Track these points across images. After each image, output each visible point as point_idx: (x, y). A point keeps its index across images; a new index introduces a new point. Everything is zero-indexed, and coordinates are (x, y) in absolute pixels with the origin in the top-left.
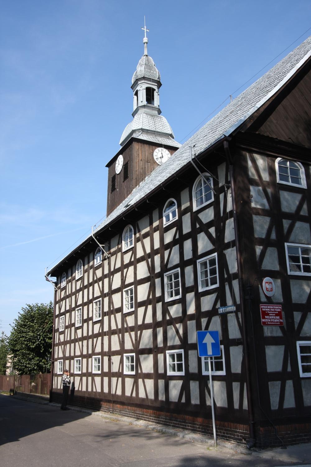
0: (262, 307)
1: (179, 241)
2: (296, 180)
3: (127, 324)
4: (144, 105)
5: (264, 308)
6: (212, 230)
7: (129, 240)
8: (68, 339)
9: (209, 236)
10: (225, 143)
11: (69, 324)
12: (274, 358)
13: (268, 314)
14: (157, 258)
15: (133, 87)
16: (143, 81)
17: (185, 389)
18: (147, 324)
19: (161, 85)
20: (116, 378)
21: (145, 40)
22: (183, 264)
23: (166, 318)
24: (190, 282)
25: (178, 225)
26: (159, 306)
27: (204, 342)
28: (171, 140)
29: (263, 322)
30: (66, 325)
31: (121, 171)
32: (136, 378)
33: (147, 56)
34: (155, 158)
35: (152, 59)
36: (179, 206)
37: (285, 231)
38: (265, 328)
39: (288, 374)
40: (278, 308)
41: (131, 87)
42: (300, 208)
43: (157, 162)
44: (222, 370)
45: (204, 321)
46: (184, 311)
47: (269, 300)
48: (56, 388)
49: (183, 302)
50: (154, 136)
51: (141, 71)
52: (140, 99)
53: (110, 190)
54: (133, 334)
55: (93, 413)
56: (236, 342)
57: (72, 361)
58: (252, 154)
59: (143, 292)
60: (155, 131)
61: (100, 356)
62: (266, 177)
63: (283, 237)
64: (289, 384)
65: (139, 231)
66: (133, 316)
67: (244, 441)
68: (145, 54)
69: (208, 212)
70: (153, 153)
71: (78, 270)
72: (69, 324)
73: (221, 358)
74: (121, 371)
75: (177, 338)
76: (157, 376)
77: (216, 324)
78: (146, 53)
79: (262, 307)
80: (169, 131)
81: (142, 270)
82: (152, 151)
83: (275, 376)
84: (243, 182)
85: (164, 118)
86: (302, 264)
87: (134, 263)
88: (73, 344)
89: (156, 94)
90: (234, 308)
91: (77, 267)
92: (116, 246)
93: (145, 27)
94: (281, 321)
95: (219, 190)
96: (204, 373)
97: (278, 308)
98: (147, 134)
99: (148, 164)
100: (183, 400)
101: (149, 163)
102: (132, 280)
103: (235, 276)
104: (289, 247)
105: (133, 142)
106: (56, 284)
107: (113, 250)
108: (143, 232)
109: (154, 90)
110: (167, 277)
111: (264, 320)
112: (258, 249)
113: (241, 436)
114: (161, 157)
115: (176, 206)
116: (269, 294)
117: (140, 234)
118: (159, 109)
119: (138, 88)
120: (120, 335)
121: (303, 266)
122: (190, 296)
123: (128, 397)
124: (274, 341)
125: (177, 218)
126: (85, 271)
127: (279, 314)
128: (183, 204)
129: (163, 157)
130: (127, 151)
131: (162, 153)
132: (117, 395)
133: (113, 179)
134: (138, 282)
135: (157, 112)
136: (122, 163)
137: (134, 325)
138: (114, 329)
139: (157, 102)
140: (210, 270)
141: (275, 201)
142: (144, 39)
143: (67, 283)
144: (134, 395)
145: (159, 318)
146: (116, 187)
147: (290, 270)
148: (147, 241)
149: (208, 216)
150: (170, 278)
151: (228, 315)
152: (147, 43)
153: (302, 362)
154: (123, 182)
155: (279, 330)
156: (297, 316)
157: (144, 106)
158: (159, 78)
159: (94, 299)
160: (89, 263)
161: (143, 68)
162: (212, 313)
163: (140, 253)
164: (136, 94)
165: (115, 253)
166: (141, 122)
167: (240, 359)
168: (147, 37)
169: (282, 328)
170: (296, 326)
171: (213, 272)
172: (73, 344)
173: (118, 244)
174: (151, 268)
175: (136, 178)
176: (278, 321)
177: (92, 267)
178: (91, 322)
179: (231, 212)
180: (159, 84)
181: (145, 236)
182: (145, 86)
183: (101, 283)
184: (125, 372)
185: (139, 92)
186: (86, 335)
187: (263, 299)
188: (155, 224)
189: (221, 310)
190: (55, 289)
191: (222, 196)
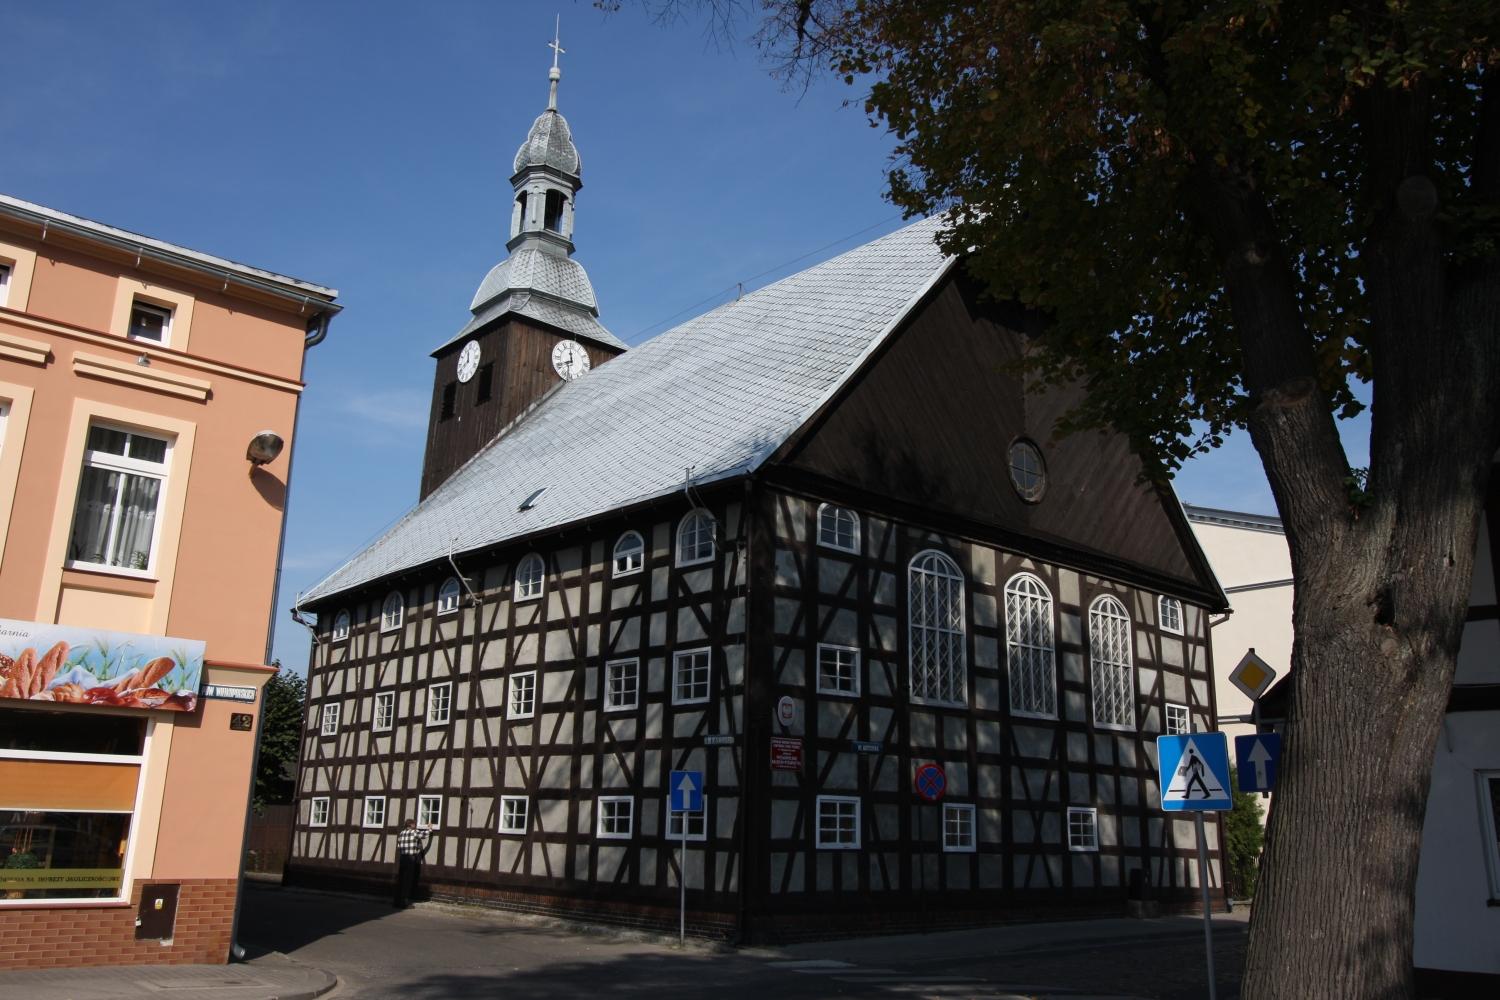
0: (775, 741)
1: (642, 609)
2: (846, 540)
3: (513, 740)
4: (539, 232)
5: (776, 742)
6: (706, 608)
7: (530, 583)
8: (349, 754)
9: (700, 616)
10: (747, 482)
11: (354, 722)
12: (782, 819)
13: (781, 753)
14: (594, 631)
15: (515, 180)
16: (543, 175)
17: (631, 861)
18: (350, 693)
19: (581, 186)
20: (479, 840)
21: (555, 72)
22: (646, 652)
23: (603, 739)
24: (656, 684)
25: (643, 582)
26: (590, 717)
27: (680, 788)
28: (591, 321)
29: (774, 765)
30: (344, 723)
31: (472, 378)
32: (526, 842)
33: (555, 112)
34: (555, 362)
35: (566, 123)
36: (648, 550)
37: (820, 623)
38: (775, 773)
39: (800, 843)
40: (797, 744)
41: (511, 180)
42: (846, 585)
43: (559, 372)
44: (701, 832)
45: (677, 754)
46: (641, 728)
47: (786, 732)
48: (303, 854)
49: (640, 717)
50: (555, 309)
51: (538, 148)
52: (531, 214)
53: (440, 409)
54: (526, 761)
55: (416, 904)
56: (727, 792)
57: (357, 803)
58: (790, 585)
59: (555, 687)
60: (558, 298)
61: (441, 797)
62: (801, 531)
63: (817, 633)
64: (800, 857)
65: (558, 572)
66: (530, 727)
67: (724, 937)
68: (550, 107)
69: (698, 577)
70: (551, 350)
71: (389, 613)
72: (354, 722)
73: (702, 814)
74: (491, 826)
75: (621, 772)
76: (571, 837)
77: (698, 759)
78: (552, 104)
79: (775, 741)
80: (591, 303)
81: (558, 646)
82: (549, 346)
83: (781, 845)
84: (766, 549)
85: (580, 267)
86: (838, 677)
87: (543, 628)
88: (364, 766)
89: (566, 207)
90: (731, 740)
91: (385, 605)
92: (498, 586)
93: (557, 42)
94: (799, 763)
95: (726, 547)
96: (669, 836)
97: (797, 744)
98: (541, 303)
99: (538, 375)
100: (625, 879)
101: (541, 374)
102: (533, 660)
103: (739, 690)
104: (822, 650)
105: (512, 323)
106: (317, 630)
107: (488, 592)
108: (567, 575)
109: (564, 197)
110: (612, 668)
111: (774, 762)
112: (778, 652)
113: (722, 931)
114: (567, 363)
115: (642, 548)
116: (785, 722)
117: (559, 578)
118: (572, 244)
119: (529, 188)
120: (496, 760)
121: (841, 680)
122: (654, 709)
123: (504, 875)
124: (785, 794)
125: (641, 569)
126: (408, 620)
127: (797, 754)
128: (657, 549)
129: (572, 362)
130: (493, 335)
131: (571, 354)
132: (480, 872)
133: (447, 393)
134: (543, 667)
135: (565, 251)
136: (477, 361)
137: (530, 744)
138: (481, 745)
139: (566, 226)
140: (696, 672)
141: (810, 574)
142: (552, 70)
143: (354, 634)
144: (520, 870)
145: (588, 736)
146: (455, 412)
147: (821, 686)
148: (574, 595)
149: (701, 582)
150: (617, 671)
151: (721, 748)
152: (557, 81)
153: (821, 826)
154: (477, 406)
155: (794, 778)
156: (823, 757)
157: (538, 235)
158: (577, 172)
159: (430, 680)
160: (421, 603)
161: (544, 143)
162: (695, 741)
163: (555, 612)
164: (523, 198)
165: (496, 599)
166: (525, 271)
167: (733, 816)
168: (558, 66)
169: (799, 775)
170: (819, 772)
171: (701, 676)
172: (364, 766)
173: (504, 584)
174: (579, 647)
175: (510, 405)
176: (794, 763)
177: (431, 614)
178: (418, 728)
179: (743, 587)
180: (577, 185)
181: (572, 583)
182: (544, 187)
183: (451, 652)
184: (503, 828)
185: (528, 198)
186: (404, 751)
187: (777, 729)
188: (595, 568)
189: (709, 740)
190: (314, 640)
191: (729, 557)
